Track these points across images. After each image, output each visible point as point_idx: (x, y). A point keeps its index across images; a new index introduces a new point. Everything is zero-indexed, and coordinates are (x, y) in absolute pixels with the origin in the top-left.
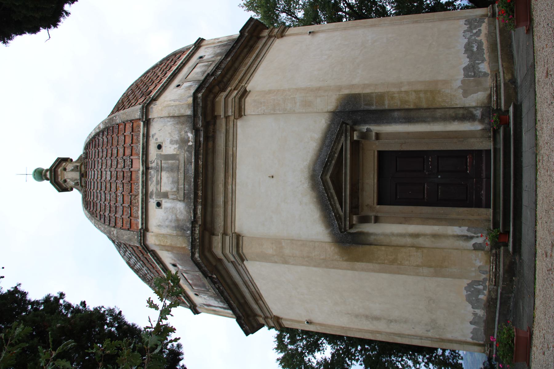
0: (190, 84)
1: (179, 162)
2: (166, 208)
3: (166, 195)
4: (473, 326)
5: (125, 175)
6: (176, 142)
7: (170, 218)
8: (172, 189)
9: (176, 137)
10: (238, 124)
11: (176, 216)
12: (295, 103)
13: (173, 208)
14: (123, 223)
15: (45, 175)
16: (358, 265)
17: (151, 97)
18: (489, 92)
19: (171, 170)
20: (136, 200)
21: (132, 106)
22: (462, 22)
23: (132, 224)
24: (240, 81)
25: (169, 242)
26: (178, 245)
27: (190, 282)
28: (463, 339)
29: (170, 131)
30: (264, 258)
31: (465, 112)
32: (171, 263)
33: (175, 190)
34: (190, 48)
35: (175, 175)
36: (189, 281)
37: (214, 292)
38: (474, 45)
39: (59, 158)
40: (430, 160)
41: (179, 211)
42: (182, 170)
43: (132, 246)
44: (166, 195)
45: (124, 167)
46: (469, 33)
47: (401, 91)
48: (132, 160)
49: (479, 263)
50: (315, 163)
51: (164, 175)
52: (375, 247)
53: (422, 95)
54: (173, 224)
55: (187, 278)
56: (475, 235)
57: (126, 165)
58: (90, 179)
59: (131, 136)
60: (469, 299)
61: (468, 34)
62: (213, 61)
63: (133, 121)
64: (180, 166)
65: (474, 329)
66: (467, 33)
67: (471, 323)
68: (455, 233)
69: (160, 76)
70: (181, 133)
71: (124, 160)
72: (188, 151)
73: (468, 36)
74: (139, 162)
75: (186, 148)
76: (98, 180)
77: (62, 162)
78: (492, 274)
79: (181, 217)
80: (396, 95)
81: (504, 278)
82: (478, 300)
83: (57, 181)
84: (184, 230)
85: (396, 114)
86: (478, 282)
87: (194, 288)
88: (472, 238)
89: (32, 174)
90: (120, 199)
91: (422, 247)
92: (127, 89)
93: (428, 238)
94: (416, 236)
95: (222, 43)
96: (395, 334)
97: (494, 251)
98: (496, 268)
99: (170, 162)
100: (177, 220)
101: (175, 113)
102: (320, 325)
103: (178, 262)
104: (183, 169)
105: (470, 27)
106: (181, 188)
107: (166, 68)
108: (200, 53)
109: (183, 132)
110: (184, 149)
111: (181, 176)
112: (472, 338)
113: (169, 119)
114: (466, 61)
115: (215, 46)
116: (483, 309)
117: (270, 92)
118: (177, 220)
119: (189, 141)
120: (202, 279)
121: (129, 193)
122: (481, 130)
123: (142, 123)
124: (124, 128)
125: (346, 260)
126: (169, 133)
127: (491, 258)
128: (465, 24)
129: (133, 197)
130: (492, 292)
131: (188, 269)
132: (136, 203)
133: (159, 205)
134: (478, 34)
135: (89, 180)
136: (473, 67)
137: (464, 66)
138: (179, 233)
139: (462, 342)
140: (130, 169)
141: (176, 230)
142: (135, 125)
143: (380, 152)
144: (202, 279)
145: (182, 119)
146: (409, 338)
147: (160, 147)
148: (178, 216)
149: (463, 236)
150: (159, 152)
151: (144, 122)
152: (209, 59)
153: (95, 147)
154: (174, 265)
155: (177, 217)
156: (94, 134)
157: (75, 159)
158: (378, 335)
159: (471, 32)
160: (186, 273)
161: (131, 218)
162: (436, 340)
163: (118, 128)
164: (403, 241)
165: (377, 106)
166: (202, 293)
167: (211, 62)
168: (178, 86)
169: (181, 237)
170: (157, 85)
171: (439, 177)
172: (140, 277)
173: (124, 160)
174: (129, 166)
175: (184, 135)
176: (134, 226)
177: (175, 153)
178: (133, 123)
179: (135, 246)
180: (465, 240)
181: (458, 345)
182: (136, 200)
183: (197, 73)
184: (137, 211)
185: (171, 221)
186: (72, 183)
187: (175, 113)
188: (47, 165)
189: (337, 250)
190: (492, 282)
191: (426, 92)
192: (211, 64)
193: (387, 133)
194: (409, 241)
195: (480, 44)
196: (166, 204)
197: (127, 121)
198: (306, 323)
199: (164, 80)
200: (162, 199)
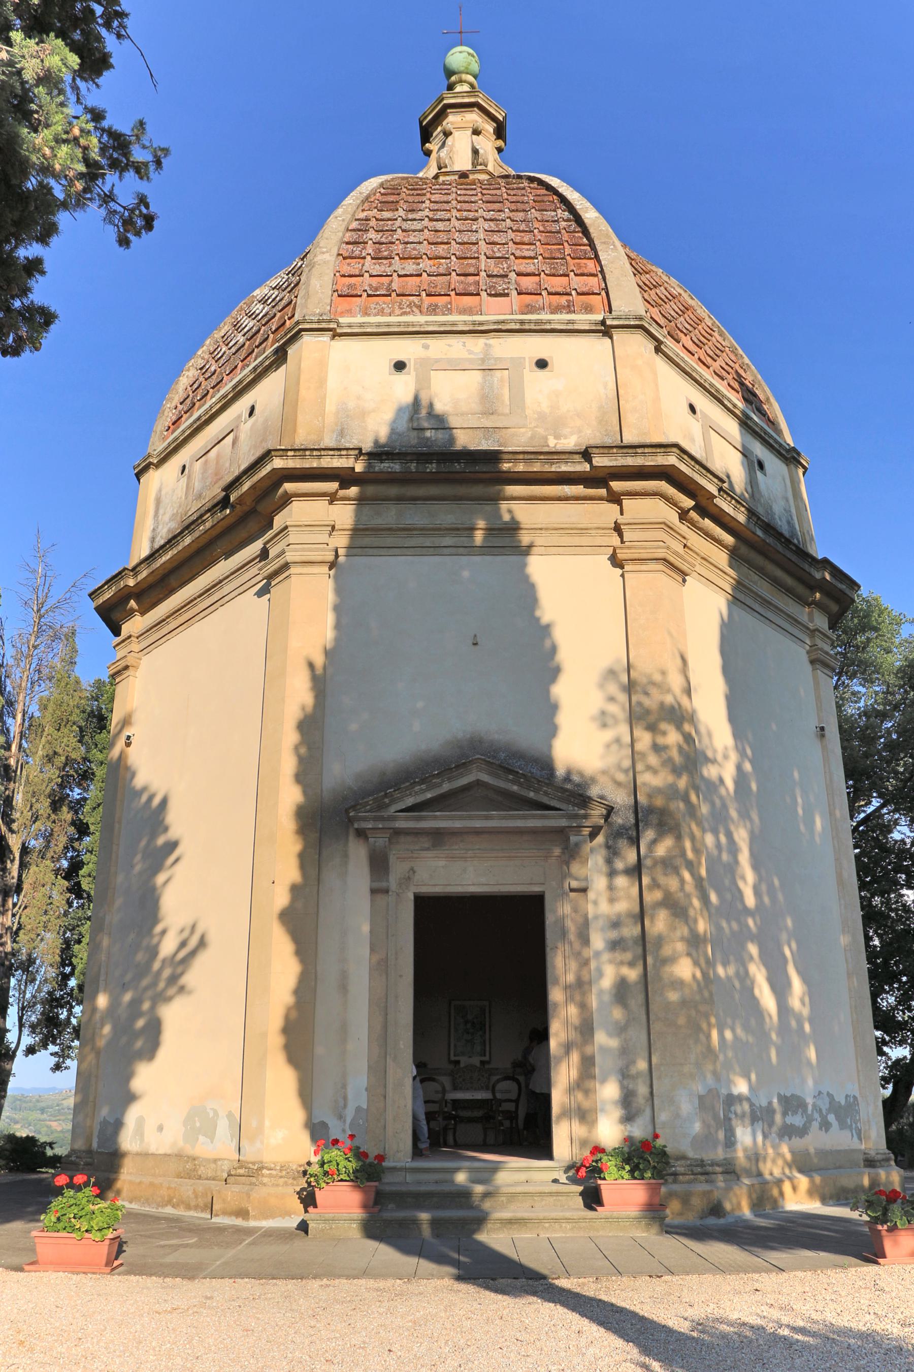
5: (471, 279)
20: (408, 310)
46: (827, 1106)
48: (507, 295)
54: (351, 405)
57: (494, 280)
66: (827, 1100)
73: (819, 1103)
75: (540, 431)
115: (787, 500)
119: (557, 437)
133: (400, 366)
142: (596, 300)
147: (542, 364)
149: (345, 1098)
150: (530, 365)
168: (692, 409)
182: (408, 310)
200: (413, 373)
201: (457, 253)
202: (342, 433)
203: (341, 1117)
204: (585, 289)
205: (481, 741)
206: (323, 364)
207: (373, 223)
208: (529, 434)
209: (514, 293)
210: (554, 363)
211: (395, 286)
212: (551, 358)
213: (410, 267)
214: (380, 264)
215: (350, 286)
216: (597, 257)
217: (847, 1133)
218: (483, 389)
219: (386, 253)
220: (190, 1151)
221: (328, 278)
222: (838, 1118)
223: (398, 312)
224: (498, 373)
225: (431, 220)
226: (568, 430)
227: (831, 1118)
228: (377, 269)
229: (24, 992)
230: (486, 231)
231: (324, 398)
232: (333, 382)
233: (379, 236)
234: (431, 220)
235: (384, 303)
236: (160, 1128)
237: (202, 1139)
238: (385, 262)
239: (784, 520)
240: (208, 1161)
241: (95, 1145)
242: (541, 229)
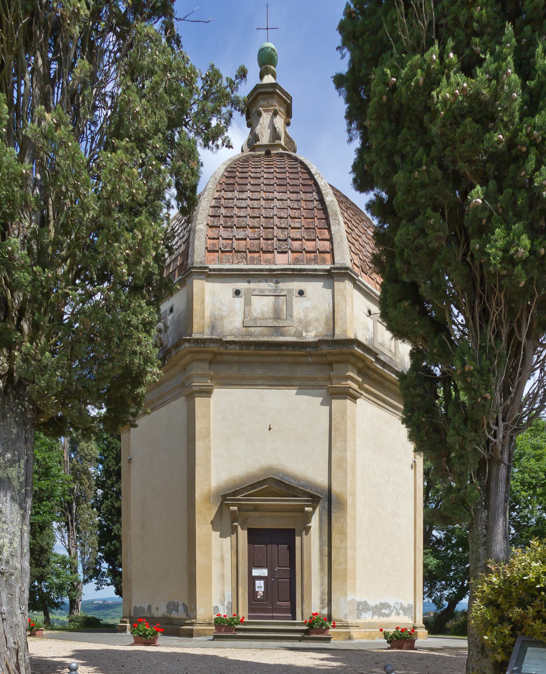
0: (370, 329)
1: (284, 320)
3: (248, 303)
4: (146, 608)
5: (270, 242)
7: (224, 308)
11: (226, 317)
13: (235, 312)
17: (360, 278)
18: (343, 620)
20: (241, 260)
24: (367, 391)
39: (290, 99)
41: (232, 320)
44: (248, 303)
45: (279, 240)
50: (286, 475)
54: (217, 313)
57: (281, 242)
61: (398, 607)
73: (397, 606)
74: (285, 264)
75: (299, 328)
77: (286, 106)
79: (226, 322)
83: (260, 97)
90: (241, 234)
103: (176, 316)
105: (405, 608)
112: (135, 607)
119: (307, 332)
121: (248, 249)
123: (328, 267)
124: (324, 238)
129: (244, 254)
132: (238, 259)
136: (367, 609)
137: (368, 602)
140: (276, 249)
142: (328, 256)
143: (294, 530)
147: (301, 293)
150: (296, 293)
151: (328, 271)
153: (303, 185)
154: (171, 310)
155: (225, 317)
159: (400, 609)
167: (394, 351)
170: (374, 280)
174: (280, 247)
182: (241, 260)
185: (220, 309)
191: (346, 569)
192: (391, 351)
195: (388, 615)
196: (239, 302)
200: (243, 297)
201: (263, 224)
202: (213, 328)
203: (223, 605)
205: (272, 469)
206: (203, 291)
207: (223, 201)
208: (295, 330)
210: (307, 293)
211: (235, 246)
212: (305, 289)
213: (241, 234)
214: (227, 231)
215: (214, 245)
216: (329, 229)
217: (407, 617)
218: (275, 306)
219: (229, 224)
220: (169, 615)
222: (403, 612)
223: (236, 261)
224: (282, 298)
225: (251, 199)
226: (312, 328)
227: (401, 612)
229: (84, 559)
230: (278, 208)
231: (204, 309)
232: (208, 299)
233: (226, 211)
234: (251, 199)
235: (230, 256)
236: (157, 609)
237: (174, 612)
238: (229, 229)
240: (176, 619)
241: (132, 615)
242: (305, 207)
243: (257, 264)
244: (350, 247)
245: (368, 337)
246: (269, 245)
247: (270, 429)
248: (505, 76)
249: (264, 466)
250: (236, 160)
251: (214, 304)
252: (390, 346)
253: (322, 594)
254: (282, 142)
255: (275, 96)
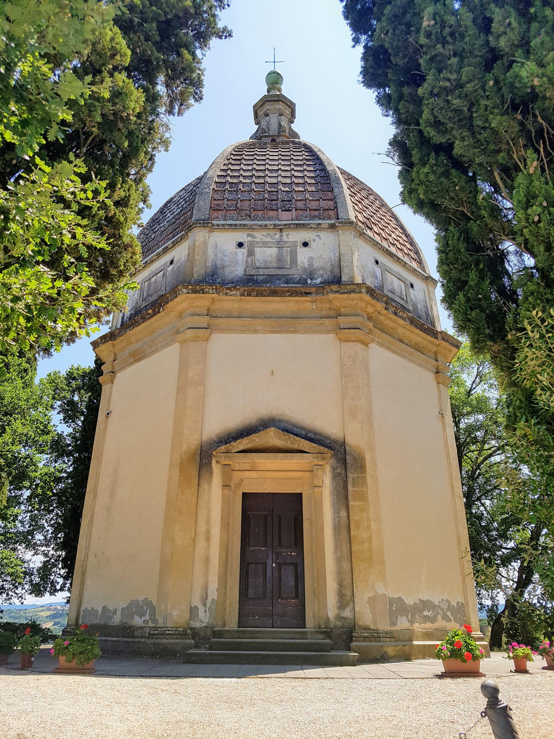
2: (236, 254)
3: (251, 253)
4: (100, 611)
5: (274, 202)
6: (311, 265)
7: (226, 259)
8: (258, 261)
9: (316, 265)
10: (331, 335)
12: (354, 400)
14: (218, 200)
15: (274, 88)
16: (176, 472)
19: (280, 259)
20: (245, 217)
21: (354, 206)
22: (460, 599)
23: (217, 211)
25: (198, 257)
26: (195, 269)
27: (153, 279)
28: (85, 599)
29: (323, 256)
30: (183, 366)
31: (348, 598)
32: (174, 258)
33: (258, 264)
34: (425, 271)
35: (275, 265)
36: (154, 278)
37: (142, 307)
38: (431, 612)
40: (293, 554)
42: (279, 272)
43: (192, 211)
44: (251, 253)
46: (447, 607)
47: (370, 521)
48: (291, 211)
49: (175, 613)
51: (273, 251)
52: (196, 490)
53: (366, 546)
54: (218, 263)
55: (158, 275)
56: (207, 608)
57: (285, 203)
58: (269, 154)
59: (319, 208)
60: (134, 603)
61: (445, 606)
62: (407, 302)
63: (336, 210)
64: (283, 270)
65: (97, 611)
66: (447, 604)
67: (105, 607)
68: (210, 584)
69: (390, 238)
70: (321, 270)
71: (290, 201)
72: (300, 279)
73: (442, 605)
75: (304, 276)
76: (267, 166)
78: (163, 629)
80: (365, 515)
81: (158, 644)
82: (132, 615)
84: (213, 276)
85: (344, 514)
86: (153, 614)
87: (146, 283)
88: (205, 605)
89: (276, 70)
91: (194, 545)
92: (378, 193)
93: (205, 552)
94: (208, 539)
95: (430, 310)
96: (92, 516)
97: (189, 632)
98: (169, 634)
99: (289, 257)
100: (223, 267)
101: (344, 262)
102: (105, 428)
103: (176, 267)
104: (280, 273)
106: (259, 272)
107: (400, 243)
108: (419, 284)
109: (322, 272)
110: (302, 274)
111: (273, 272)
113: (337, 254)
114: (409, 601)
115: (426, 301)
116: (121, 621)
117: (367, 371)
118: (223, 267)
120: (157, 294)
122: (328, 616)
125: (181, 458)
126: (321, 256)
127: (181, 628)
128: (458, 602)
130: (141, 631)
131: (169, 279)
133: (240, 245)
134: (446, 618)
135: (268, 152)
137: (404, 598)
138: (209, 270)
139: (81, 597)
141: (212, 266)
142: (332, 213)
144: (157, 294)
145: (337, 271)
146: (88, 533)
147: (305, 244)
148: (228, 268)
149: (207, 595)
150: (300, 244)
152: (410, 296)
154: (172, 263)
156: (322, 158)
157: (293, 126)
158: (92, 496)
160: (163, 276)
161: (224, 211)
162: (84, 566)
163: (328, 191)
164: (202, 521)
165: (352, 491)
166: (140, 293)
167: (405, 298)
168: (377, 262)
169: (204, 272)
171: (274, 565)
172: (155, 215)
173: (290, 201)
175: (319, 273)
176: (215, 214)
177: (299, 263)
178: (333, 210)
179: (192, 214)
180: (202, 596)
181: (78, 593)
182: (245, 217)
183: (392, 283)
184: (232, 219)
185: (222, 260)
186: (264, 124)
187: (344, 262)
188: (286, 90)
189: (193, 447)
190: (154, 630)
192: (403, 299)
193: (322, 503)
194: (202, 529)
196: (242, 252)
197: (336, 202)
198: (108, 412)
199: (385, 244)
200: (247, 248)
204: (327, 207)
209: (294, 210)
221: (208, 201)
228: (231, 197)
239: (424, 313)
243: (261, 220)
244: (354, 206)
245: (376, 285)
246: (273, 205)
247: (272, 374)
248: (469, 409)
249: (265, 416)
250: (244, 144)
251: (215, 255)
252: (402, 293)
253: (339, 585)
254: (287, 134)
255: (281, 102)
